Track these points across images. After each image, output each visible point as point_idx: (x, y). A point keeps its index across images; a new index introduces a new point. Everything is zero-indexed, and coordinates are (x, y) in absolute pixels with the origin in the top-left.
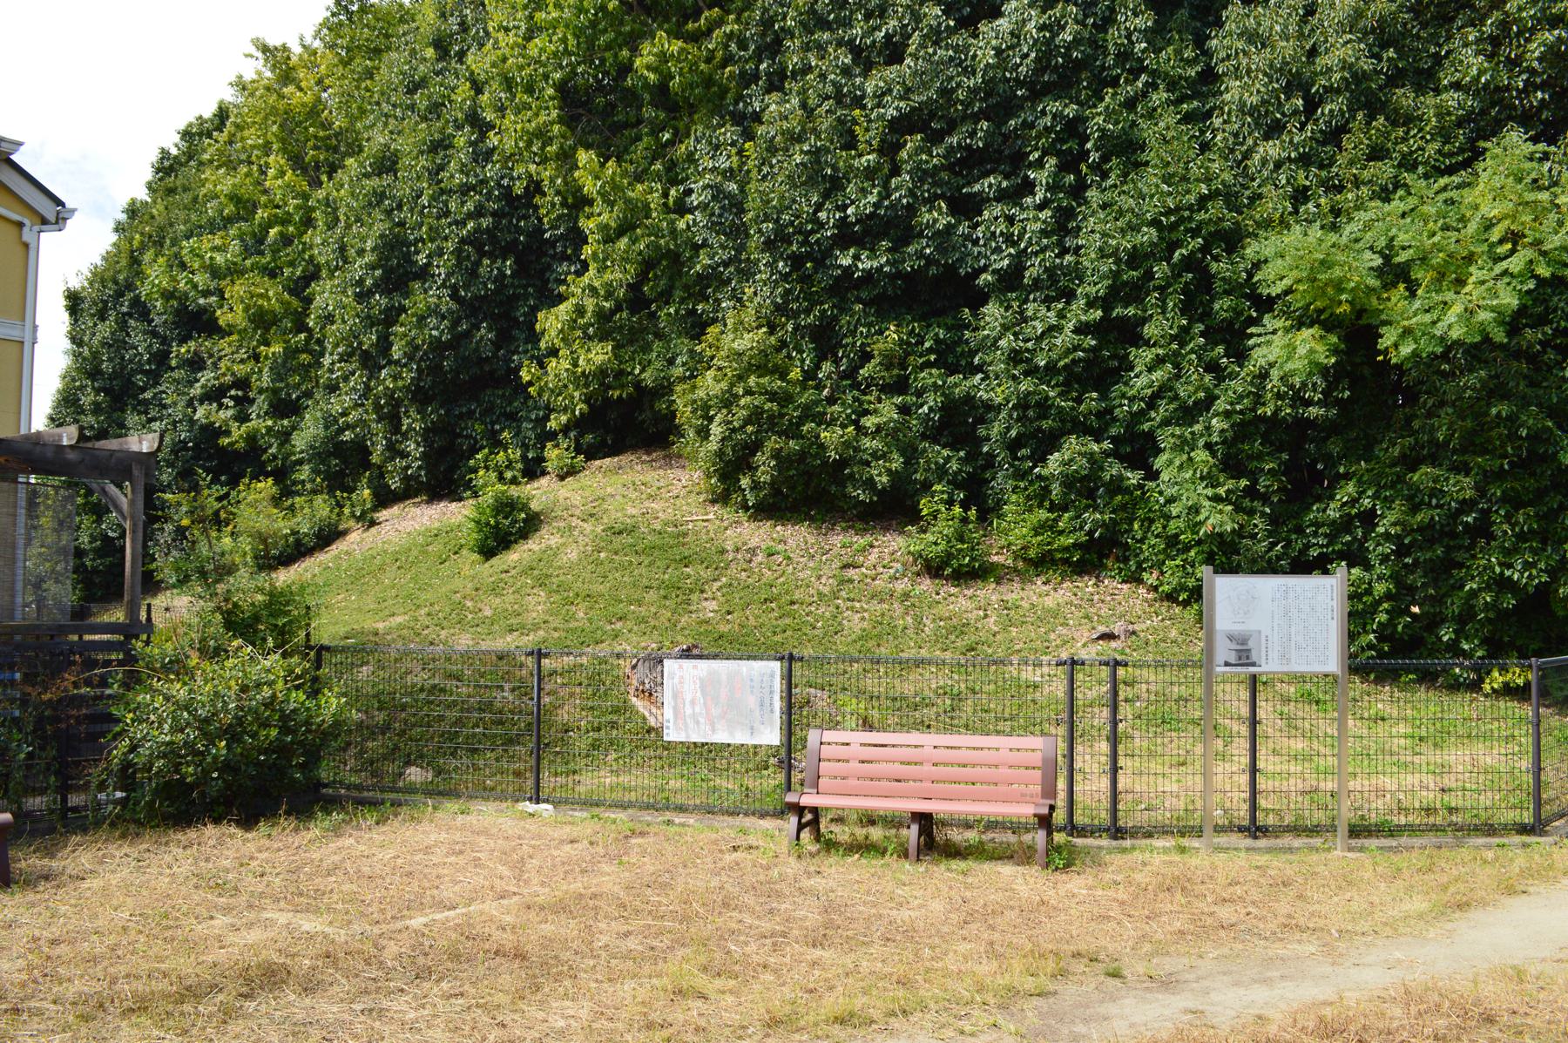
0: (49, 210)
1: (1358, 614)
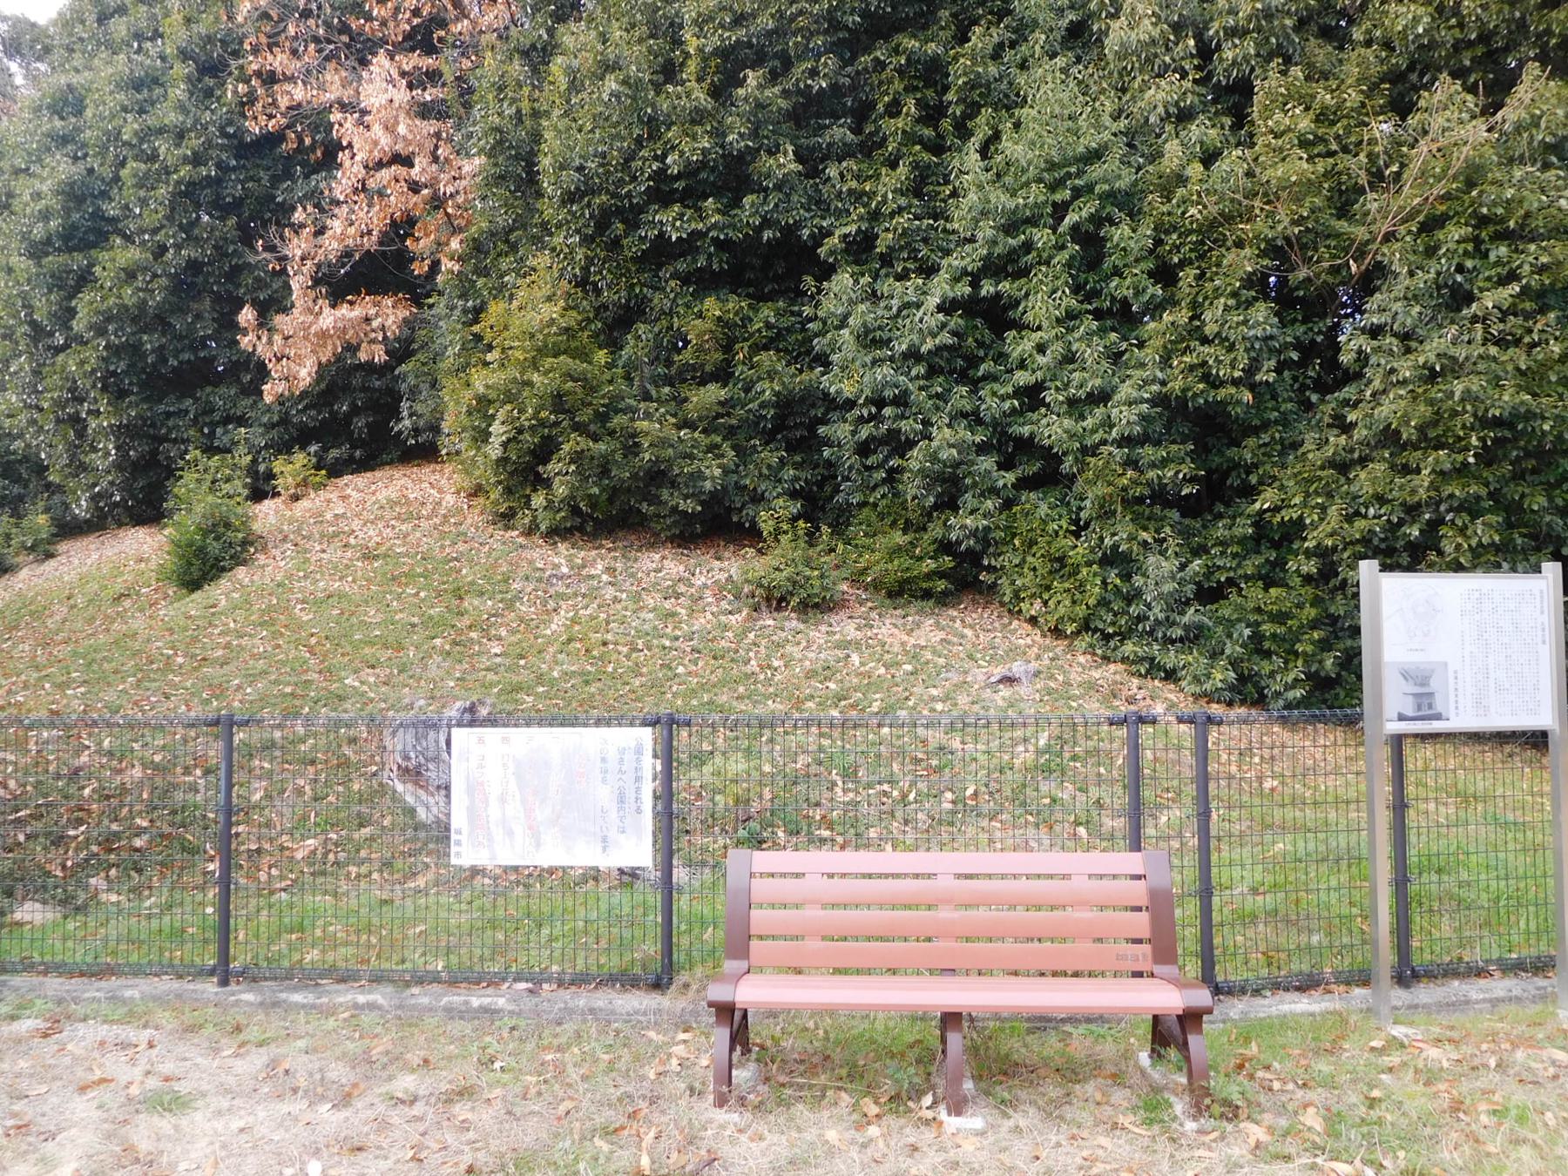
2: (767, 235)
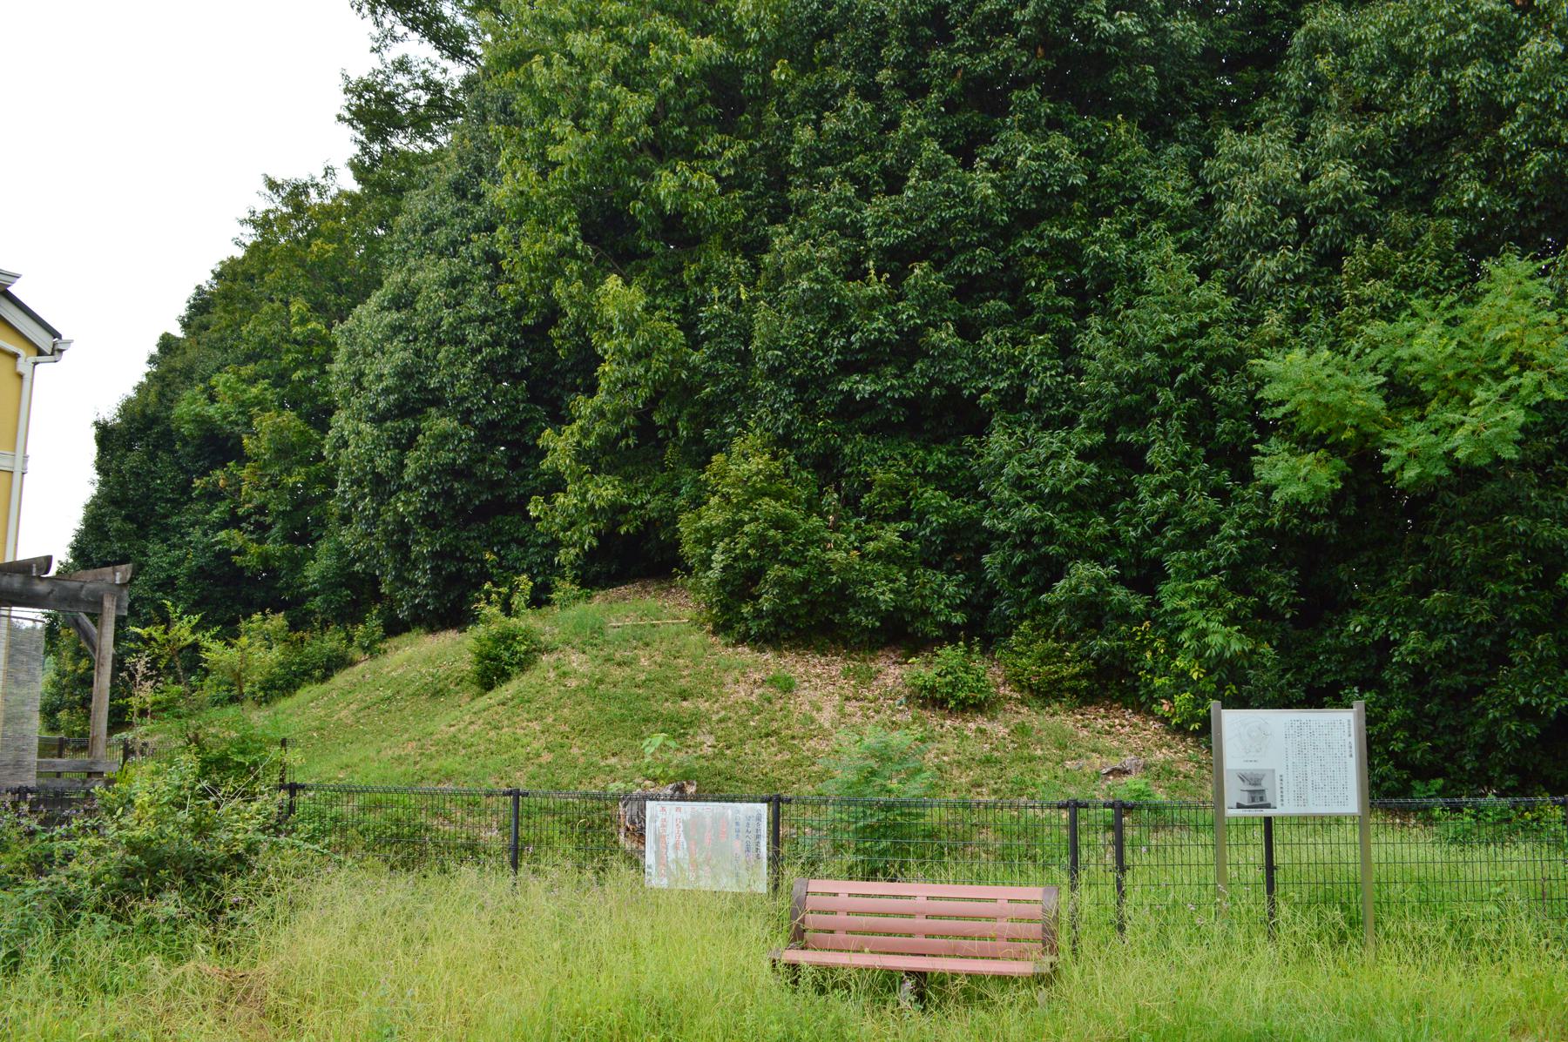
0: (45, 342)
1: (1375, 746)
2: (935, 391)
